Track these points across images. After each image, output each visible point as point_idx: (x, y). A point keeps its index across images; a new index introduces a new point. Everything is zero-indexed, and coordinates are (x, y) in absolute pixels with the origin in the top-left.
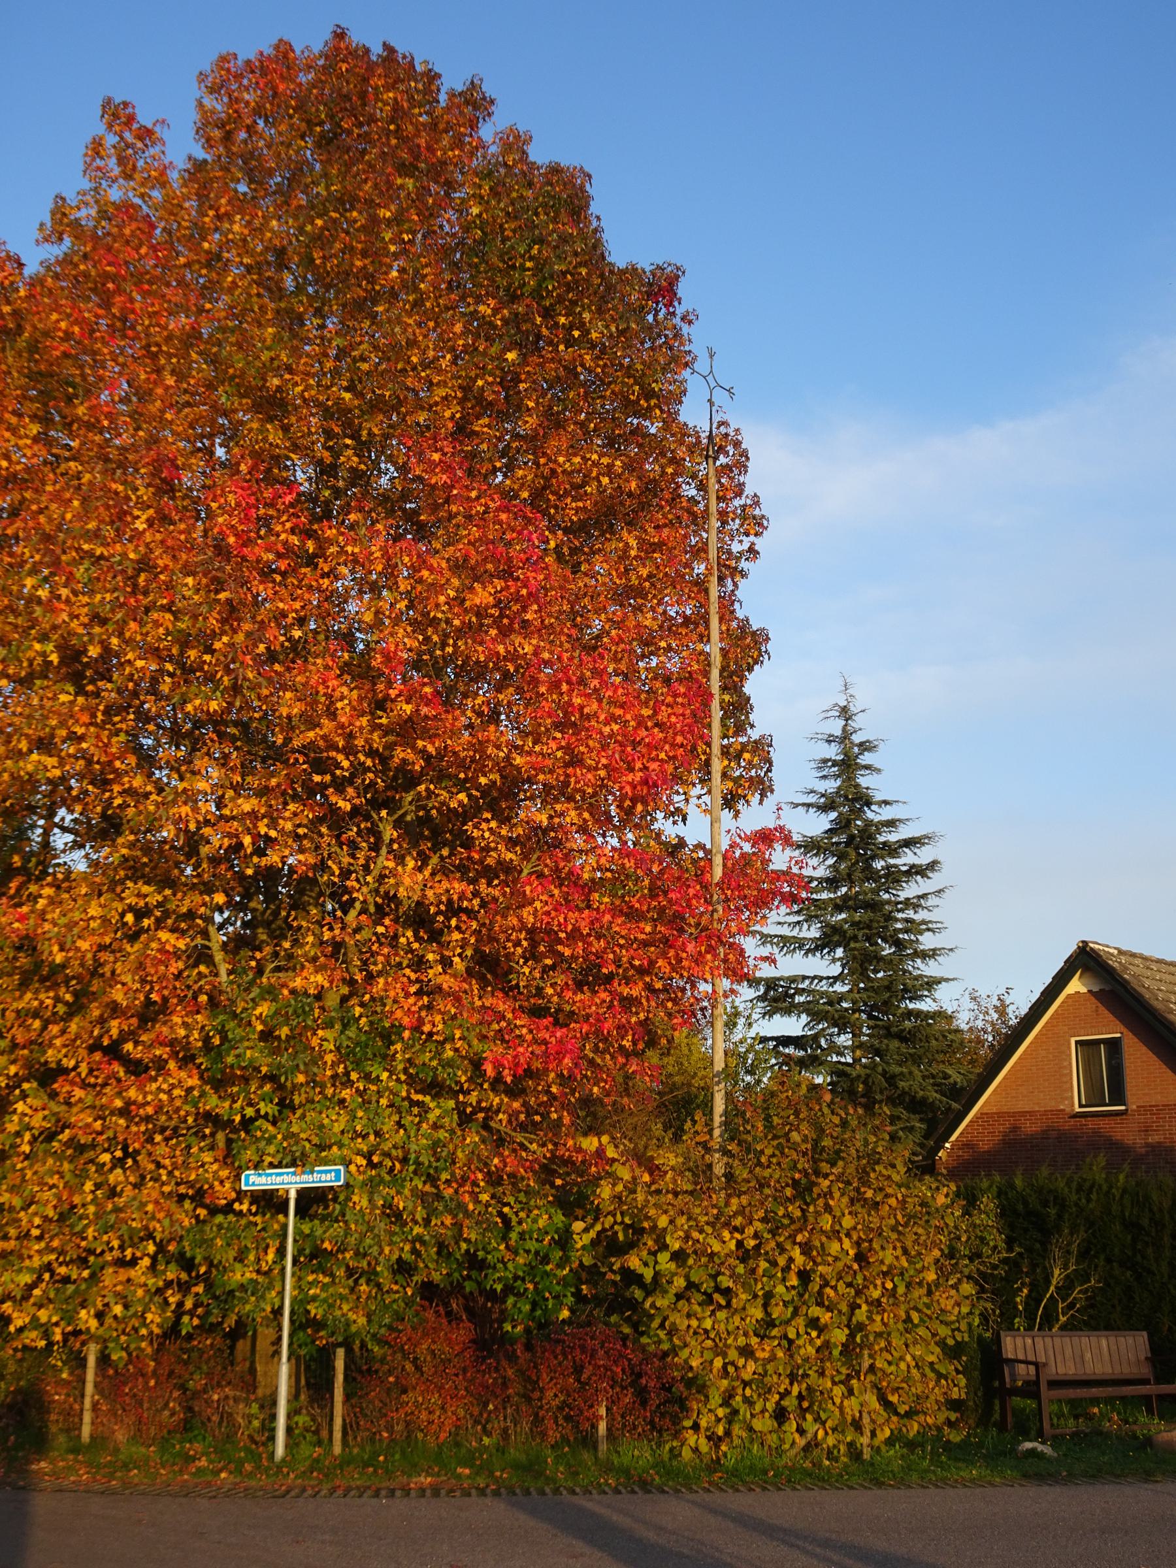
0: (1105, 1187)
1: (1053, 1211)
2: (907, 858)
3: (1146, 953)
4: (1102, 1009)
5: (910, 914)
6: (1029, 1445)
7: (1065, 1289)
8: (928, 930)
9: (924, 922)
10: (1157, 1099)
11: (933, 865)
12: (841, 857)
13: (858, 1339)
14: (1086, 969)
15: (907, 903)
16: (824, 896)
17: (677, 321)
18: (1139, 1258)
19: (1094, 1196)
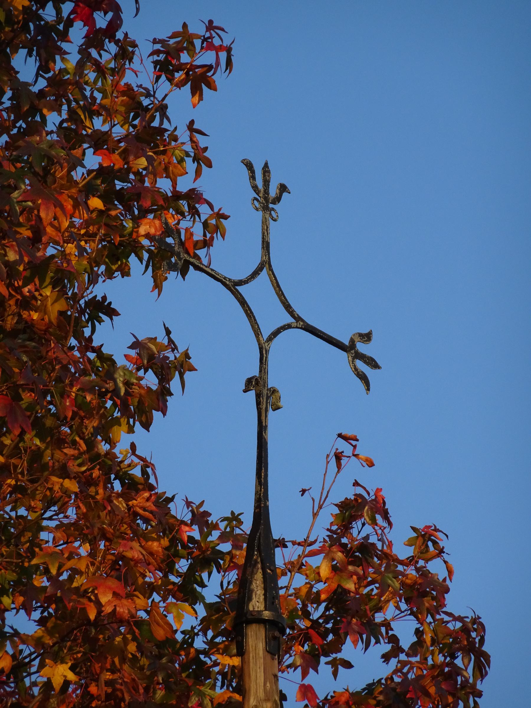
17: (140, 73)
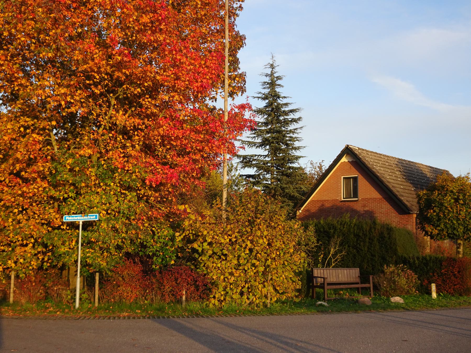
0: (349, 224)
1: (332, 231)
2: (291, 116)
3: (367, 149)
5: (291, 135)
6: (320, 302)
7: (334, 255)
8: (297, 140)
9: (296, 138)
10: (368, 196)
11: (299, 119)
12: (269, 115)
14: (348, 154)
16: (263, 128)
19: (345, 226)
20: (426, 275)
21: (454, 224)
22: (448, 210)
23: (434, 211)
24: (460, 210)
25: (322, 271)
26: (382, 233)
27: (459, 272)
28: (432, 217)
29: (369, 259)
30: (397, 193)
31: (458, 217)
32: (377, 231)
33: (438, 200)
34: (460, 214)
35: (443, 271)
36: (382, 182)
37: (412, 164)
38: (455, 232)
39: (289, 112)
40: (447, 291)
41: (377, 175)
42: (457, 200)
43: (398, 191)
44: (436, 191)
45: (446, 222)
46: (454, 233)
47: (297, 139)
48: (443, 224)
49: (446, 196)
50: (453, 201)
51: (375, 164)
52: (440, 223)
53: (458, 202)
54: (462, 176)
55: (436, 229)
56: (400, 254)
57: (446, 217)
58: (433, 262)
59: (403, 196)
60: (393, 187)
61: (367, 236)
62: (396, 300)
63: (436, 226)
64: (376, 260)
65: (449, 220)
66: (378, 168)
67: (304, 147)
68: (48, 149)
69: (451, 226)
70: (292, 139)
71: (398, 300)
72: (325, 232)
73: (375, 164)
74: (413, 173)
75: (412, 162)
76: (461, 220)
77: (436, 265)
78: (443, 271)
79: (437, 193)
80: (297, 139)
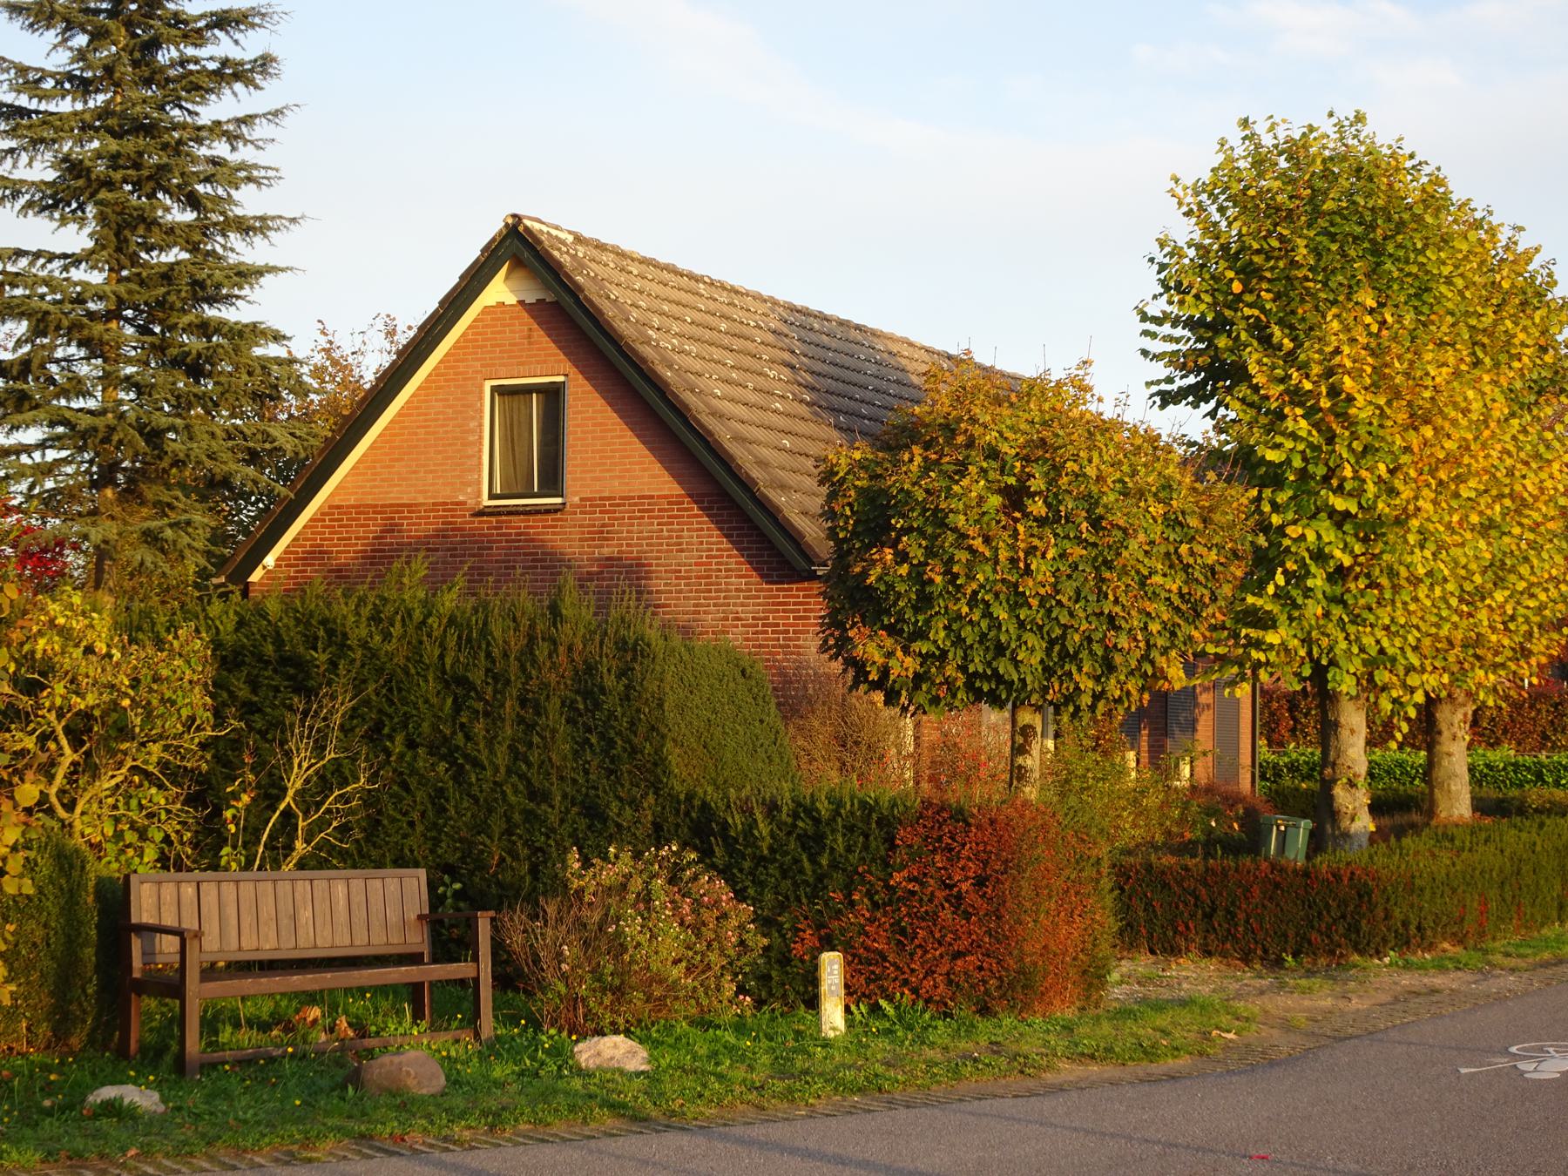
0: (418, 615)
1: (322, 657)
2: (222, 47)
3: (625, 246)
4: (540, 336)
5: (221, 149)
6: (108, 1092)
7: (308, 800)
8: (249, 179)
9: (243, 166)
10: (615, 487)
11: (265, 63)
12: (99, 36)
13: (824, 862)
14: (518, 263)
15: (216, 129)
16: (65, 106)
18: (460, 739)
19: (396, 631)
20: (811, 898)
21: (996, 624)
22: (970, 549)
23: (902, 557)
24: (1030, 551)
25: (189, 891)
26: (590, 669)
27: (980, 882)
28: (890, 587)
29: (517, 817)
30: (755, 473)
31: (1016, 585)
32: (562, 657)
33: (920, 495)
34: (1028, 571)
35: (897, 877)
36: (681, 412)
37: (855, 335)
38: (1003, 666)
39: (209, 27)
40: (915, 991)
41: (659, 377)
42: (1015, 497)
43: (762, 463)
44: (917, 450)
45: (959, 617)
46: (995, 671)
47: (246, 174)
48: (941, 622)
49: (963, 473)
50: (995, 501)
51: (656, 321)
52: (927, 622)
53: (1020, 506)
54: (1057, 375)
55: (906, 651)
56: (680, 789)
57: (959, 588)
58: (850, 829)
59: (783, 487)
60: (738, 438)
61: (508, 682)
62: (607, 1053)
63: (907, 636)
64: (553, 819)
65: (973, 601)
66: (669, 346)
67: (293, 220)
68: (1190, 670)
69: (983, 636)
70: (217, 169)
71: (618, 1053)
72: (285, 661)
73: (656, 321)
74: (855, 377)
75: (858, 328)
76: (1035, 602)
77: (866, 847)
78: (897, 877)
79: (918, 460)
80: (246, 174)
